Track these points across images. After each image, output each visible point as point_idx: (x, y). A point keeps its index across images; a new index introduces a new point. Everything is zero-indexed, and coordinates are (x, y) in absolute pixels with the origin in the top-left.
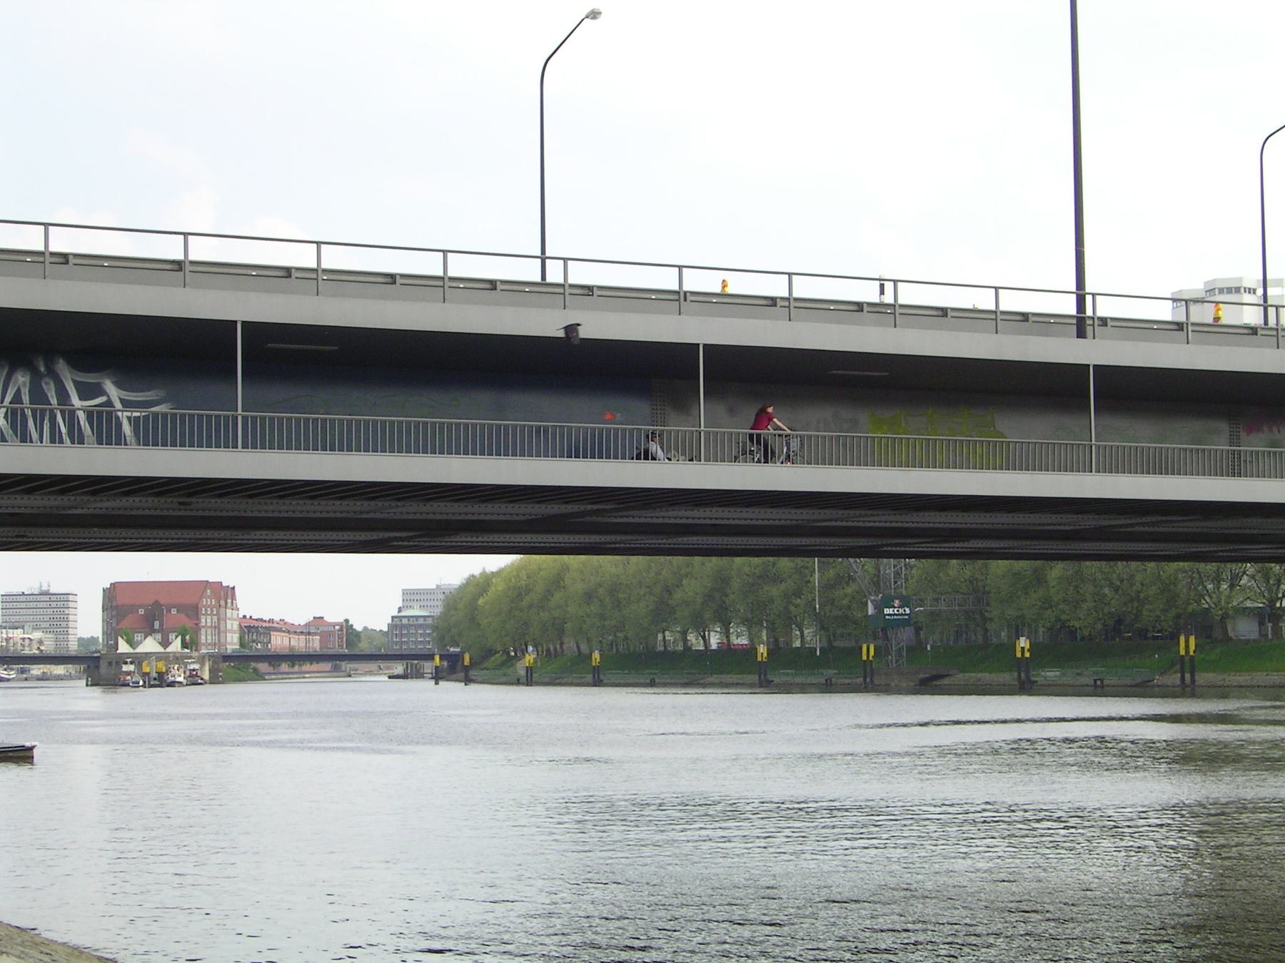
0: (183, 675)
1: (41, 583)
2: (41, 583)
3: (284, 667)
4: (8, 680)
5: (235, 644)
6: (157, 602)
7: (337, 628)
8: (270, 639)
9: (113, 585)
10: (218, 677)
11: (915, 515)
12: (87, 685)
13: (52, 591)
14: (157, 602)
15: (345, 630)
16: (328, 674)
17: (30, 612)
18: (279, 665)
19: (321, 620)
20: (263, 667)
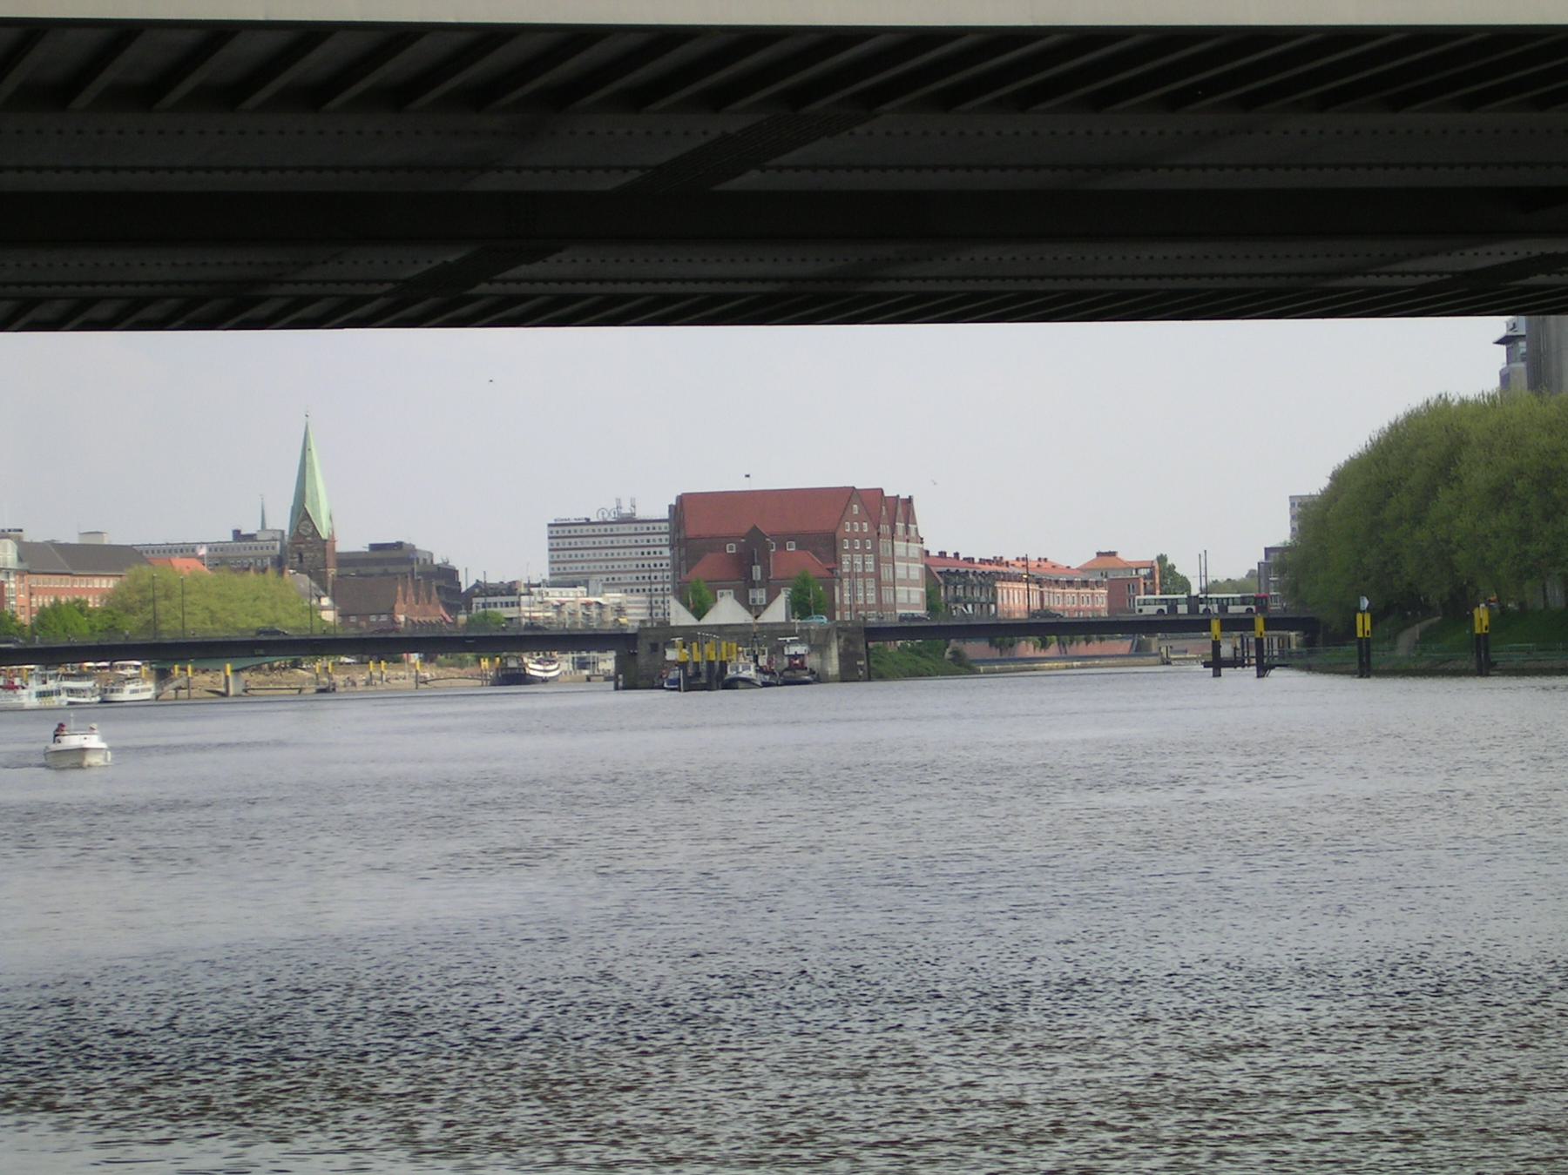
0: (752, 666)
1: (618, 500)
2: (618, 500)
3: (1027, 648)
4: (545, 680)
5: (916, 606)
6: (755, 529)
7: (1143, 572)
8: (995, 595)
9: (682, 499)
10: (856, 668)
11: (1469, 253)
12: (617, 688)
13: (640, 515)
14: (755, 529)
15: (1157, 576)
16: (1126, 661)
17: (602, 554)
18: (1011, 645)
19: (1112, 558)
20: (974, 649)
